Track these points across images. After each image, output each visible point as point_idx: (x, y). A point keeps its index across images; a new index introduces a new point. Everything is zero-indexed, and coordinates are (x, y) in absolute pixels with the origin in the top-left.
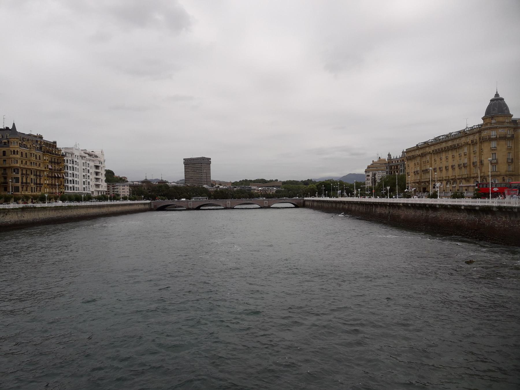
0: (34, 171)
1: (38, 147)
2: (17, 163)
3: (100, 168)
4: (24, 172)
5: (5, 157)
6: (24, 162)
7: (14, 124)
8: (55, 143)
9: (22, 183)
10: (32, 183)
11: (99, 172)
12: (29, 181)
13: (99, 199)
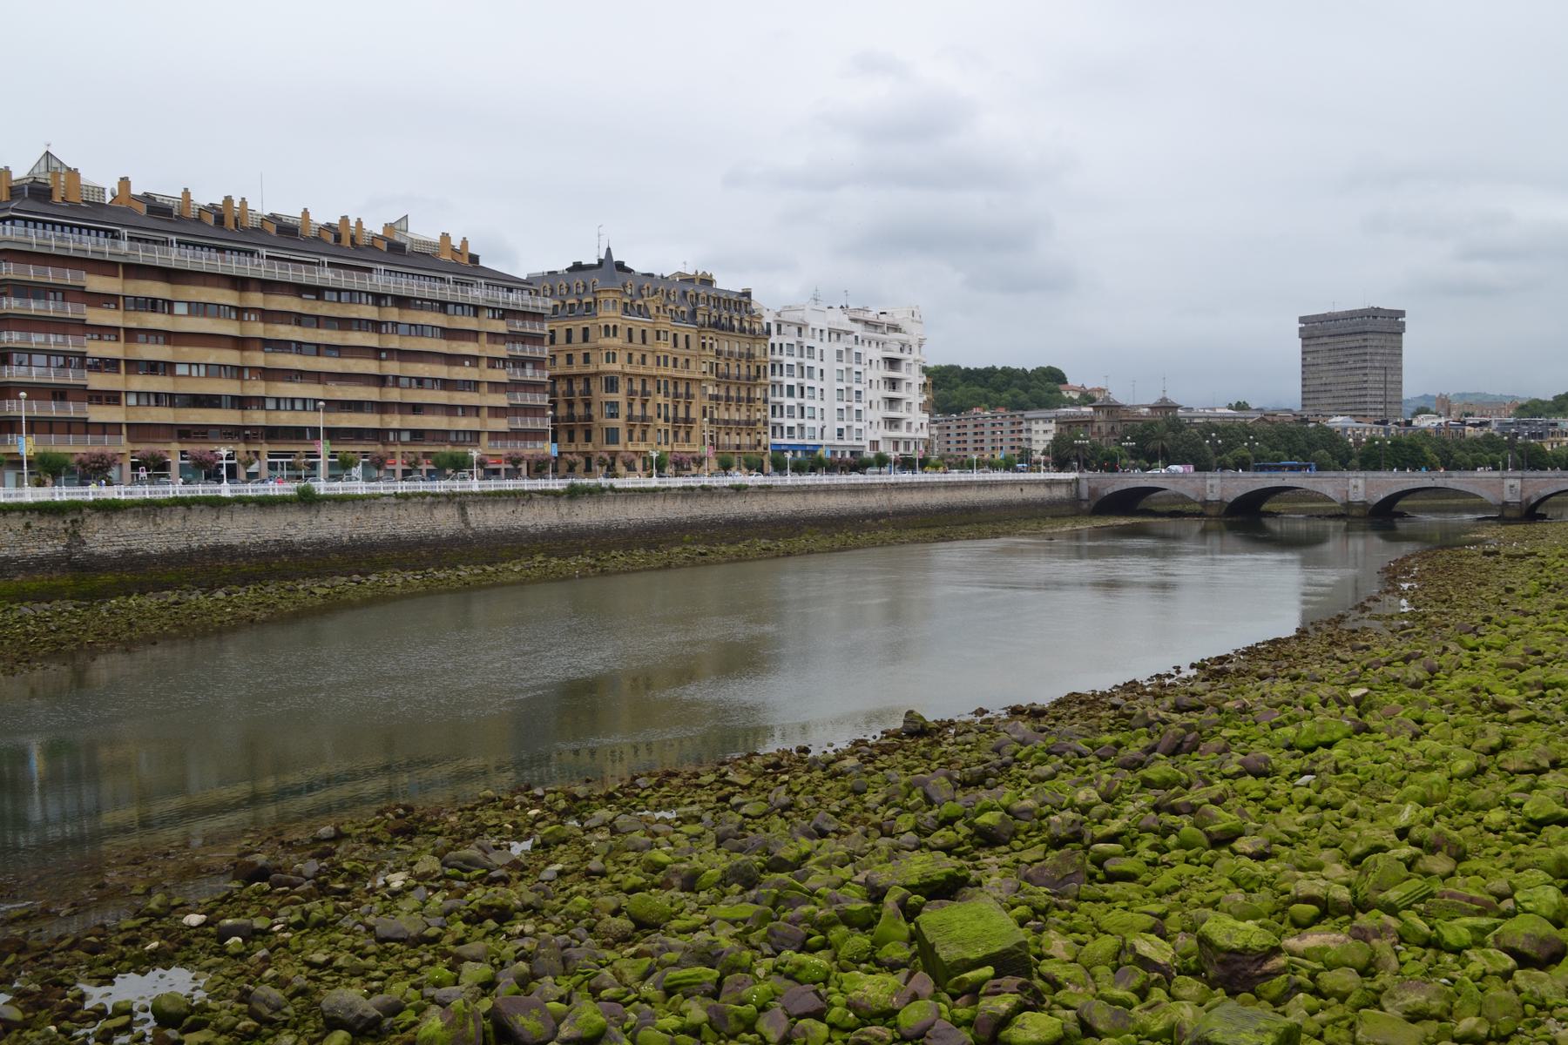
0: (666, 382)
1: (683, 312)
2: (614, 362)
3: (903, 365)
4: (637, 386)
5: (586, 345)
6: (637, 356)
7: (609, 249)
8: (747, 294)
9: (630, 418)
10: (659, 416)
11: (900, 380)
12: (651, 411)
13: (906, 464)
